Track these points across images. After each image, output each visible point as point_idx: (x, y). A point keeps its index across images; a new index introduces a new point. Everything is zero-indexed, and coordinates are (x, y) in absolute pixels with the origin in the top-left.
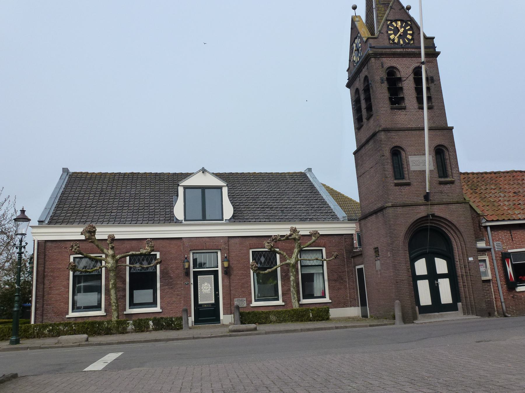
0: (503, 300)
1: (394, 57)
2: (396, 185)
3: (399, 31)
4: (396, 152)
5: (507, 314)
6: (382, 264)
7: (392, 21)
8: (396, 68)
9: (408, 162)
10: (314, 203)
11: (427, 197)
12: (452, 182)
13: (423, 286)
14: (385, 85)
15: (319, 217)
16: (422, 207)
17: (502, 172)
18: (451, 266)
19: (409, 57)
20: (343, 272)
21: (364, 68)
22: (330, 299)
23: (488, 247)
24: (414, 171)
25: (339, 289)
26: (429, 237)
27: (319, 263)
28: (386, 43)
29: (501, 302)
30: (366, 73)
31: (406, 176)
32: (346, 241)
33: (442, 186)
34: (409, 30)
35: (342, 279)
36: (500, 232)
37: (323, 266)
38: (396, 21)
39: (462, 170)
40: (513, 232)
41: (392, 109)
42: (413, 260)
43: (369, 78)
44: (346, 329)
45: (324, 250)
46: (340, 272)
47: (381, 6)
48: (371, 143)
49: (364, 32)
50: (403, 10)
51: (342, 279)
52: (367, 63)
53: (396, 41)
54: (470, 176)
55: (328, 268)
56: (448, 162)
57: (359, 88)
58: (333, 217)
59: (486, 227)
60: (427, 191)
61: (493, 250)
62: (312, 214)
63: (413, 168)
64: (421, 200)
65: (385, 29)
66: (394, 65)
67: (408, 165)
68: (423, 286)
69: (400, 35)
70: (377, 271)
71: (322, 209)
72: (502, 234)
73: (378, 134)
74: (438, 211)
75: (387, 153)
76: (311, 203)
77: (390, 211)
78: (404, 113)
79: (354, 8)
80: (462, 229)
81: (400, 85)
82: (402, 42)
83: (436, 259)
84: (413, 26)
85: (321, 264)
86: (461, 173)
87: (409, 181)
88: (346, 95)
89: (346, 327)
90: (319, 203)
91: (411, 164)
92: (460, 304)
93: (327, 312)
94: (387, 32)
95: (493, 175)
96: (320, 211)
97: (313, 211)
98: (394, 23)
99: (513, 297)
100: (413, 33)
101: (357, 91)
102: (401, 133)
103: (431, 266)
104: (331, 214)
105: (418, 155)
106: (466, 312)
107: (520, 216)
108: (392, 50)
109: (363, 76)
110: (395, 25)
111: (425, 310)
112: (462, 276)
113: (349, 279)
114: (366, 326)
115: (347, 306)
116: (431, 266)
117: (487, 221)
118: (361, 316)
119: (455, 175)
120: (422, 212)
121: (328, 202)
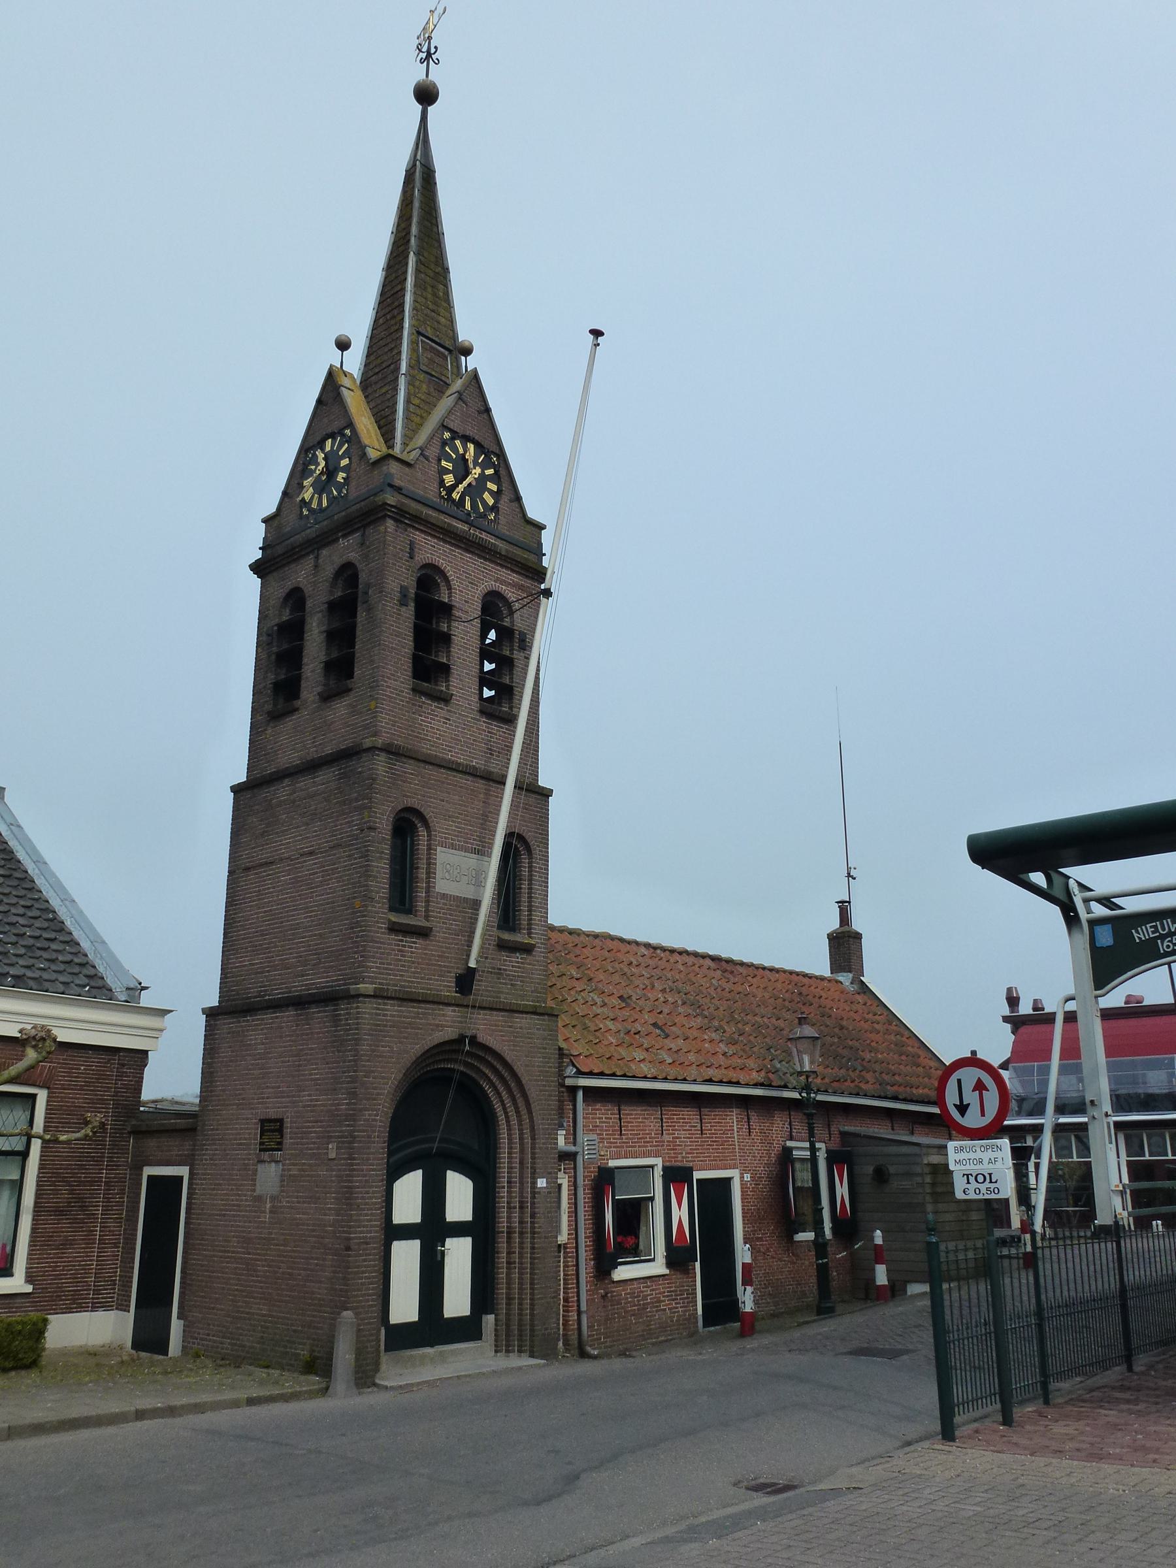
0: (584, 1307)
1: (445, 541)
2: (394, 929)
3: (467, 473)
4: (407, 825)
5: (588, 1349)
6: (286, 1180)
7: (455, 435)
8: (442, 573)
9: (430, 864)
10: (22, 921)
11: (466, 981)
12: (528, 949)
13: (406, 1257)
14: (409, 612)
15: (45, 976)
16: (449, 1011)
17: (584, 933)
18: (484, 1200)
19: (480, 557)
20: (92, 1183)
21: (345, 536)
22: (29, 1279)
23: (572, 1148)
24: (444, 896)
25: (67, 1244)
26: (450, 1110)
27: (17, 1144)
28: (431, 492)
29: (579, 1313)
30: (353, 556)
31: (421, 906)
32: (121, 1075)
33: (504, 955)
34: (490, 478)
35: (83, 1208)
36: (598, 1106)
37: (24, 1154)
38: (466, 439)
39: (556, 917)
40: (626, 1110)
41: (414, 690)
42: (395, 1172)
43: (363, 577)
44: (169, 1421)
45: (42, 1096)
46: (80, 1183)
47: (422, 376)
48: (326, 778)
49: (368, 430)
50: (485, 416)
51: (83, 1208)
52: (365, 526)
53: (456, 496)
54: (582, 938)
55: (41, 1167)
56: (525, 886)
57: (308, 590)
58: (93, 984)
59: (573, 1090)
60: (472, 964)
61: (579, 1159)
62: (21, 962)
63: (443, 885)
64: (447, 988)
65: (433, 452)
66: (442, 563)
67: (430, 873)
68: (406, 1257)
69: (470, 485)
70: (259, 1199)
71: (54, 946)
72: (605, 1114)
73: (365, 757)
74: (488, 1029)
75: (384, 823)
76: (14, 919)
77: (367, 1009)
78: (443, 713)
79: (343, 345)
80: (533, 1093)
81: (444, 627)
82: (468, 506)
83: (450, 1174)
84: (503, 472)
85: (20, 1147)
86: (552, 928)
87: (427, 924)
88: (246, 595)
89: (171, 1411)
90: (38, 924)
91: (439, 873)
92: (489, 1320)
93: (39, 1331)
94: (440, 460)
95: (708, 962)
96: (45, 955)
97: (22, 951)
98: (458, 442)
99: (604, 1297)
100: (499, 491)
101: (296, 598)
102: (429, 771)
103: (434, 1197)
104: (85, 971)
105: (460, 848)
106: (503, 1345)
107: (645, 1069)
108: (442, 517)
109: (338, 561)
110: (461, 451)
111: (404, 1338)
112: (510, 1233)
113: (106, 1209)
114: (235, 1404)
115: (81, 1308)
116: (434, 1197)
117: (580, 1073)
118: (129, 1344)
119: (536, 930)
120: (446, 1024)
121: (68, 923)
